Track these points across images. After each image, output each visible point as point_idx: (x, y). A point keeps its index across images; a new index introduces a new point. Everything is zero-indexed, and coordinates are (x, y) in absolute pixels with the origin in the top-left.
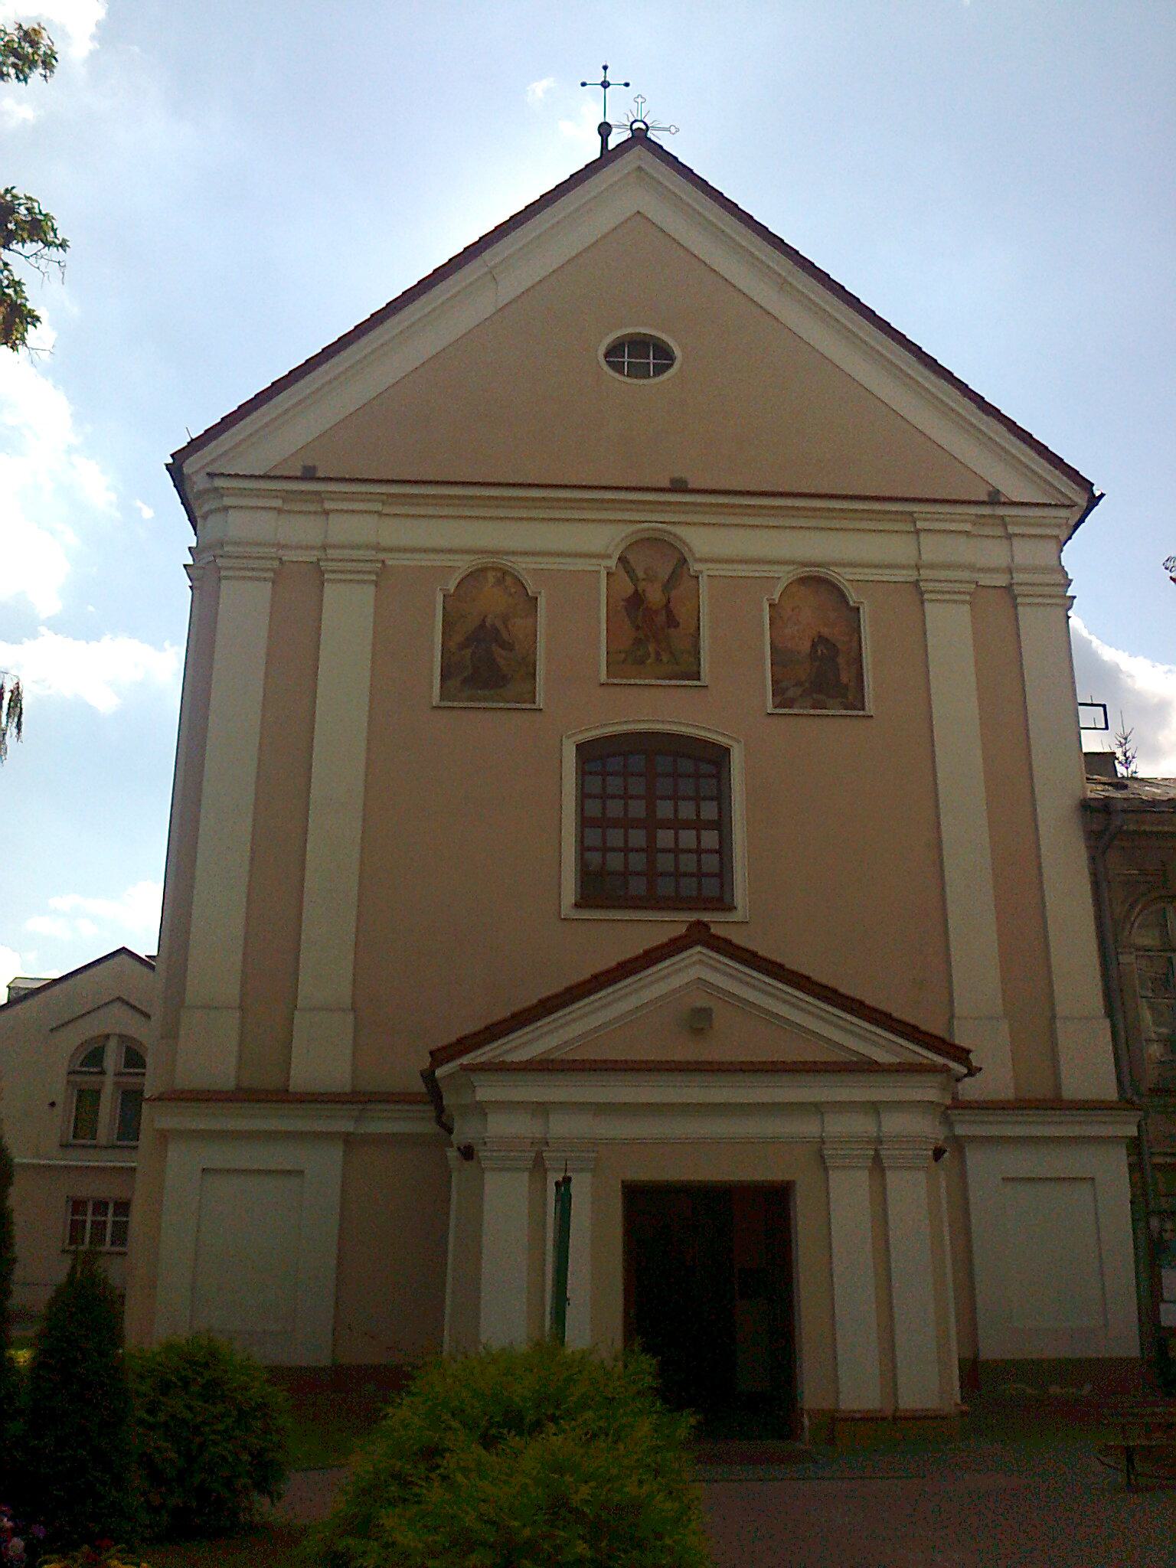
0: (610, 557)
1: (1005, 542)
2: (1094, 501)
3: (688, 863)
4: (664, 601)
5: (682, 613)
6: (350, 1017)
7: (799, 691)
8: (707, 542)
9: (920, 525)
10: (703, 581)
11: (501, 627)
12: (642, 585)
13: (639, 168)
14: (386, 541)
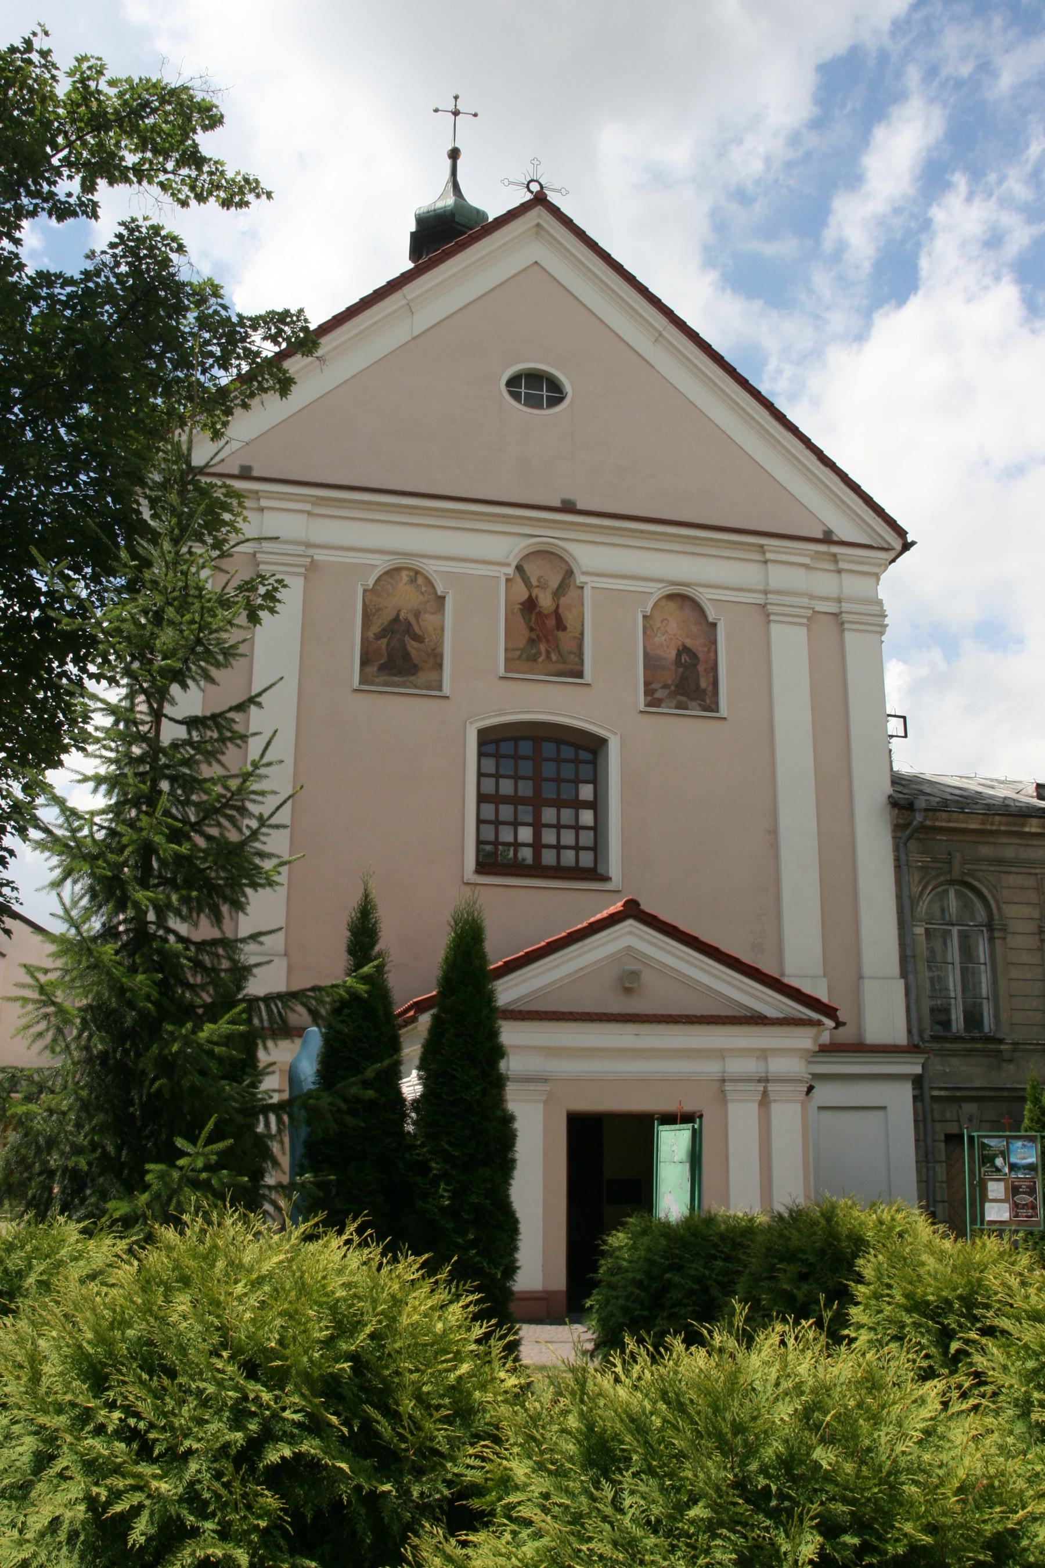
0: (509, 565)
1: (835, 575)
2: (907, 546)
3: (568, 837)
4: (554, 607)
7: (666, 692)
8: (594, 557)
9: (769, 556)
10: (588, 593)
12: (535, 592)
13: (538, 225)
14: (315, 539)
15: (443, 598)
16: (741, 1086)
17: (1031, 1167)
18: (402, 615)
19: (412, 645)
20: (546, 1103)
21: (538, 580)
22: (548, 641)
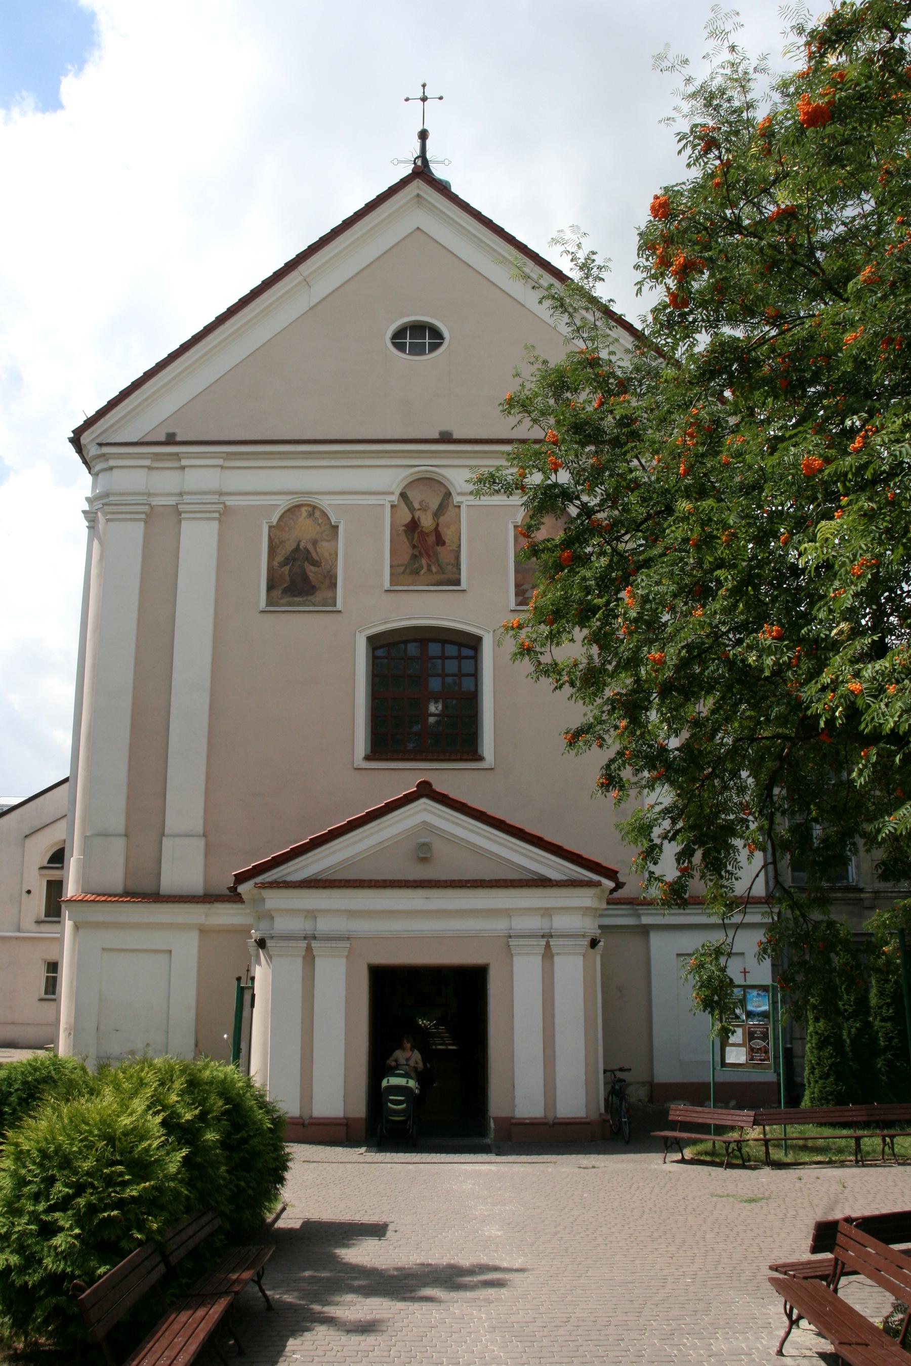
0: (392, 493)
4: (433, 527)
5: (448, 534)
6: (201, 842)
11: (310, 548)
12: (417, 514)
13: (418, 195)
15: (336, 528)
16: (567, 942)
17: (764, 1015)
18: (302, 545)
19: (310, 569)
20: (347, 957)
21: (420, 503)
22: (429, 556)
